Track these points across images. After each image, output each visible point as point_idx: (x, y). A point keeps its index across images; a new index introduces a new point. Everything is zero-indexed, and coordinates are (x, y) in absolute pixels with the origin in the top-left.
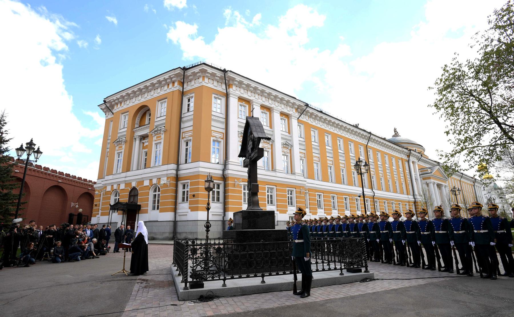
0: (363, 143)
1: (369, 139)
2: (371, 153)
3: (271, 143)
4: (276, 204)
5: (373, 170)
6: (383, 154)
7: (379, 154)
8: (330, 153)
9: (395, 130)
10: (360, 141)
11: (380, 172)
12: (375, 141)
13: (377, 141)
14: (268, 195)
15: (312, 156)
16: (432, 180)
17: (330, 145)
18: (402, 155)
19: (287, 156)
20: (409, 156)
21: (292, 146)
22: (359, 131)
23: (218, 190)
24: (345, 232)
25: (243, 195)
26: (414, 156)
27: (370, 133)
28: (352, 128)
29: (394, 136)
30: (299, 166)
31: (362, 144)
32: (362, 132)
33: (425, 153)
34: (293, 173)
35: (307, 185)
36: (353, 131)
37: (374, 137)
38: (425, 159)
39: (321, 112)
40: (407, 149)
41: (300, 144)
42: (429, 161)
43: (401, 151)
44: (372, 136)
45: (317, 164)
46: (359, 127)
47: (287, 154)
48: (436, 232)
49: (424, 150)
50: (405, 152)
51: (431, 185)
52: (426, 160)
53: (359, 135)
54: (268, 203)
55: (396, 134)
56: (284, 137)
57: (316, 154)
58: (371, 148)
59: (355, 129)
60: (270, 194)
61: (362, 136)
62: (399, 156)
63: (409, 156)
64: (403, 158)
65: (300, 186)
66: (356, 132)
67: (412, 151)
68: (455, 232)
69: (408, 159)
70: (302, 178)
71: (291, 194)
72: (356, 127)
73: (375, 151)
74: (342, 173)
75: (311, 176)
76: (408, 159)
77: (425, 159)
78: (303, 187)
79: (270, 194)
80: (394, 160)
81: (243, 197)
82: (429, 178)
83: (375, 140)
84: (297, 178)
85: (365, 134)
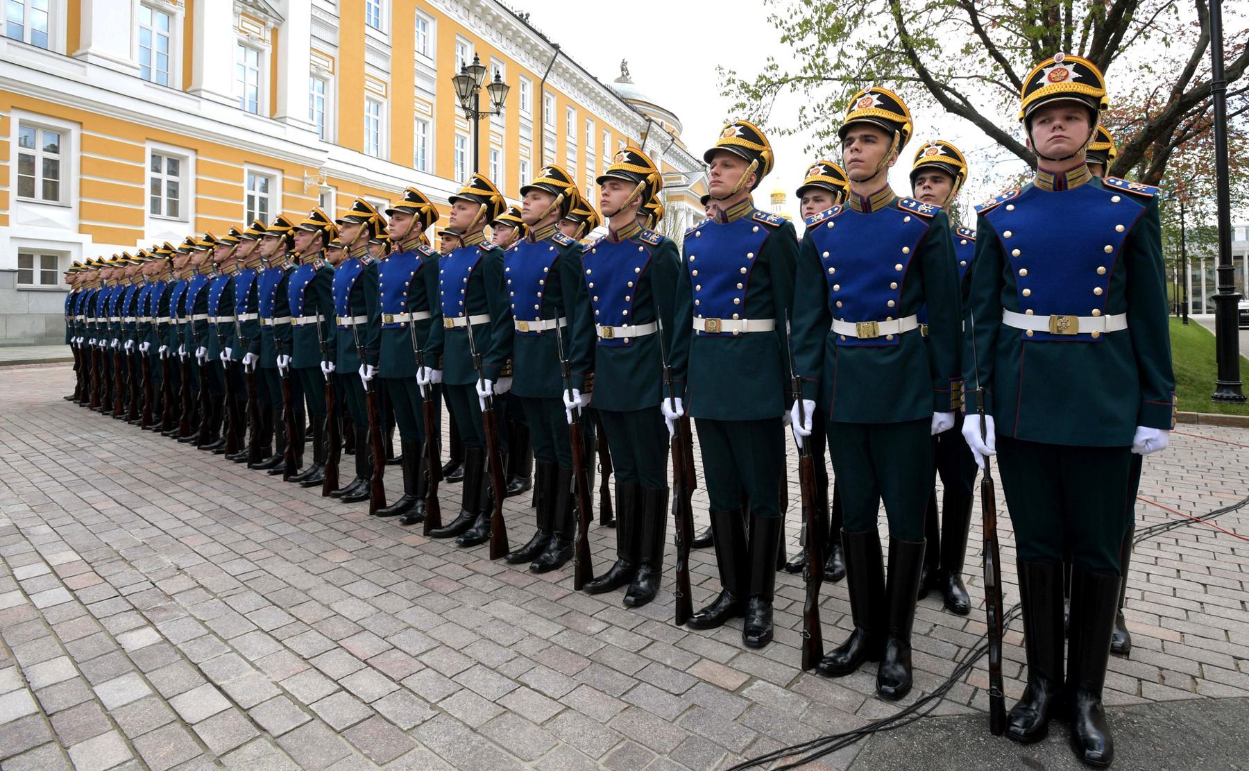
0: (535, 71)
1: (551, 66)
2: (551, 107)
3: (271, 24)
4: (191, 217)
5: (551, 155)
6: (585, 115)
7: (574, 115)
8: (591, 161)
9: (624, 64)
10: (526, 65)
11: (588, 172)
12: (564, 74)
13: (579, 81)
14: (251, 199)
15: (362, 76)
16: (684, 204)
17: (385, 26)
18: (630, 130)
19: (259, 52)
20: (644, 136)
21: (281, 19)
22: (525, 32)
23: (173, 178)
24: (401, 318)
25: (245, 203)
26: (657, 138)
27: (556, 47)
28: (506, 18)
29: (618, 81)
30: (299, 92)
31: (530, 75)
32: (535, 39)
33: (681, 138)
34: (275, 114)
35: (329, 164)
36: (507, 26)
37: (566, 63)
38: (679, 151)
39: (595, 79)
40: (643, 115)
41: (314, 19)
42: (688, 157)
43: (628, 118)
44: (559, 58)
45: (378, 104)
46: (531, 21)
47: (259, 44)
48: (699, 324)
49: (680, 131)
50: (638, 124)
51: (681, 215)
52: (682, 153)
53: (522, 44)
54: (156, 207)
55: (625, 76)
56: (318, 14)
57: (376, 67)
58: (555, 92)
59: (517, 25)
60: (258, 194)
61: (532, 51)
62: (622, 131)
63: (644, 136)
64: (632, 137)
65: (303, 167)
66: (516, 34)
67: (653, 125)
68: (843, 328)
69: (641, 143)
70: (314, 141)
71: (265, 189)
72: (522, 19)
73: (566, 104)
74: (492, 161)
75: (351, 138)
76: (641, 143)
77: (679, 151)
78: (313, 171)
79: (258, 194)
80: (592, 130)
81: (246, 211)
82: (681, 198)
83: (566, 70)
84: (291, 134)
85: (543, 46)
